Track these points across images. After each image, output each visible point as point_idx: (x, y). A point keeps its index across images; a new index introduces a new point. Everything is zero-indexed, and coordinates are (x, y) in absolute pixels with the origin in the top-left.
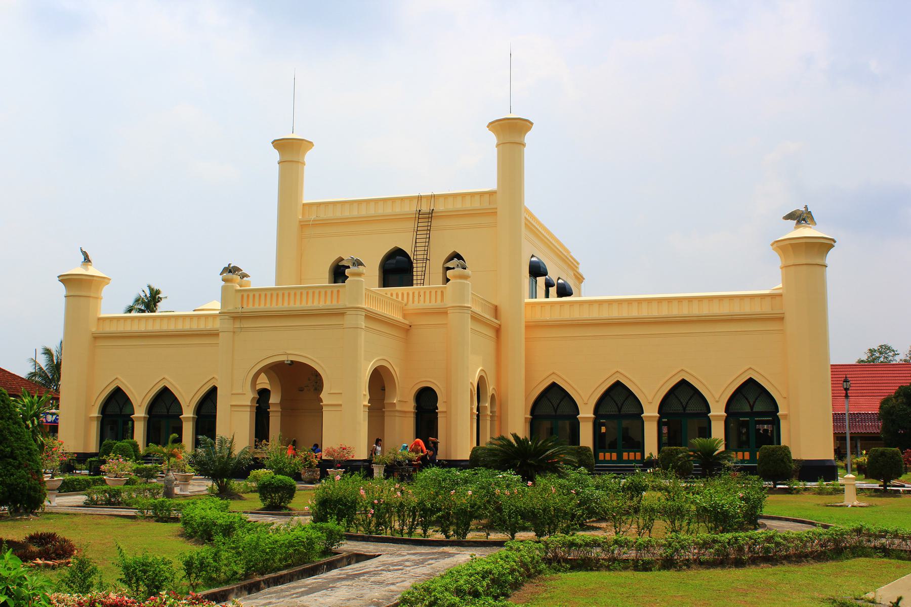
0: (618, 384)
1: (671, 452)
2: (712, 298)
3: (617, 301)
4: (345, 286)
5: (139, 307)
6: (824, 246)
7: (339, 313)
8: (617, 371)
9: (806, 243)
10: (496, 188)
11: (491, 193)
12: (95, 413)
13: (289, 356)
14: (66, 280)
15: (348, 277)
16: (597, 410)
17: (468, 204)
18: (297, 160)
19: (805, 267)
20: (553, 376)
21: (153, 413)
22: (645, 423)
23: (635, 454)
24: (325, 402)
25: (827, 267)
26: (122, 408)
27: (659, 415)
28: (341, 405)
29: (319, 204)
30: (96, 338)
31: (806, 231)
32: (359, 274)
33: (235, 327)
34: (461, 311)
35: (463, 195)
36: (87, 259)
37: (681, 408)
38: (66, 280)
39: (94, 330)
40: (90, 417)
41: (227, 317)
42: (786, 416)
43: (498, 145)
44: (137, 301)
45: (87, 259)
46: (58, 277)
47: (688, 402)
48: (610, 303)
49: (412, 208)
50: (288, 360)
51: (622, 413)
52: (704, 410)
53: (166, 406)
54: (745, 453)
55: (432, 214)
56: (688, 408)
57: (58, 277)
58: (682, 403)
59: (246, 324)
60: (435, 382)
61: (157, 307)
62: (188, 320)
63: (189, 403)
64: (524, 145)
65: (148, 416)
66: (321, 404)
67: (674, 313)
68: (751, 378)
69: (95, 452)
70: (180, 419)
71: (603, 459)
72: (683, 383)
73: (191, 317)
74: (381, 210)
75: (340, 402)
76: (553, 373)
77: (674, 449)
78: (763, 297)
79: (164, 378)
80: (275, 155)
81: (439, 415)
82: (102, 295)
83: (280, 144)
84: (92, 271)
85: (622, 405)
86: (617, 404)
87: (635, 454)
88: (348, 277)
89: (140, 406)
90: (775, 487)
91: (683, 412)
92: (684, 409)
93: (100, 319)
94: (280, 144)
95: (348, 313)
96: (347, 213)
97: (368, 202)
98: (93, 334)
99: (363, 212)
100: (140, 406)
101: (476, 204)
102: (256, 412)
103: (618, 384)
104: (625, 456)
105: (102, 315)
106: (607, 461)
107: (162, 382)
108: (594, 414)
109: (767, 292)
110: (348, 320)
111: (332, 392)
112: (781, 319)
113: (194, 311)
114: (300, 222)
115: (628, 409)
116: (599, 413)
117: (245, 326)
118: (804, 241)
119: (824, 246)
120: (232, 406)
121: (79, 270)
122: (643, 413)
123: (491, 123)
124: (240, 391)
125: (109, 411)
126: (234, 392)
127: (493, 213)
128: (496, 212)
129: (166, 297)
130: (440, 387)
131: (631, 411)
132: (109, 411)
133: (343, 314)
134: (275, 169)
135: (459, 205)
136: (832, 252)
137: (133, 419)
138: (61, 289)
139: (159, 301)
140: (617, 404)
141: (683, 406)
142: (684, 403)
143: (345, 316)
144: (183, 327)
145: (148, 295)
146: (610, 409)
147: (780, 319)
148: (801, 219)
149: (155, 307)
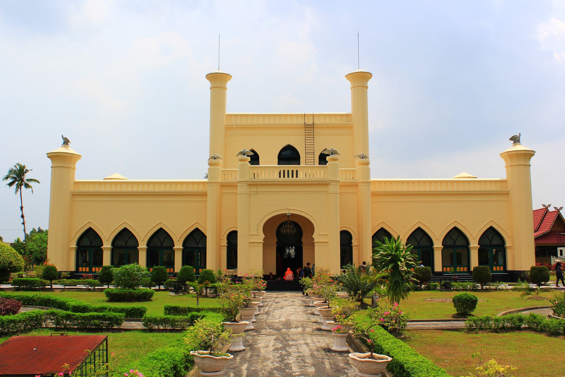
0: (161, 230)
1: (541, 269)
2: (166, 183)
3: (451, 181)
4: (327, 167)
5: (12, 176)
6: (529, 155)
7: (325, 184)
8: (383, 222)
9: (525, 153)
10: (351, 112)
11: (347, 115)
12: (74, 246)
13: (290, 210)
14: (53, 156)
15: (328, 162)
16: (113, 243)
17: (333, 121)
18: (224, 87)
19: (523, 166)
20: (125, 224)
21: (80, 245)
22: (139, 252)
23: (464, 268)
24: (316, 240)
25: (530, 166)
26: (92, 242)
27: (182, 247)
28: (328, 242)
29: (237, 115)
30: (74, 195)
31: (518, 147)
32: (336, 160)
33: (250, 190)
34: (210, 185)
35: (286, 116)
36: (66, 142)
37: (453, 243)
38: (53, 156)
39: (72, 190)
40: (71, 248)
41: (245, 184)
42: (510, 247)
43: (211, 88)
44: (11, 172)
45: (66, 142)
46: (47, 154)
47: (456, 239)
48: (374, 182)
49: (301, 121)
50: (289, 214)
51: (163, 246)
52: (464, 243)
53: (125, 241)
54: (497, 267)
55: (313, 125)
56: (456, 243)
57: (47, 154)
58: (453, 240)
59: (260, 189)
60: (350, 227)
61: (24, 176)
62: (174, 186)
63: (180, 239)
64: (367, 87)
65: (112, 247)
66: (314, 241)
67: (140, 190)
68: (197, 228)
69: (74, 270)
70: (137, 249)
71: (81, 271)
72: (197, 230)
73: (100, 183)
74: (283, 121)
75: (327, 240)
76: (455, 221)
77: (542, 267)
78: (496, 182)
79: (197, 223)
80: (208, 84)
81: (353, 248)
82: (76, 166)
83: (212, 77)
84: (70, 150)
85: (163, 241)
86: (417, 241)
87: (464, 268)
88: (328, 162)
89: (179, 241)
90: (482, 287)
91: (161, 246)
92: (454, 243)
93: (76, 183)
94: (212, 77)
95: (332, 184)
96: (255, 122)
97: (269, 116)
98: (72, 192)
99: (266, 121)
100: (179, 241)
101: (338, 121)
102: (228, 247)
103: (161, 230)
104: (94, 269)
105: (77, 180)
106: (171, 273)
107: (124, 224)
108: (183, 246)
109: (498, 179)
110: (332, 188)
111: (321, 233)
112: (507, 194)
113: (104, 179)
114: (225, 126)
115: (131, 243)
116: (115, 245)
117: (259, 191)
118: (524, 152)
119: (529, 155)
120: (250, 242)
121: (63, 150)
122: (174, 246)
123: (207, 75)
124: (256, 233)
125: (82, 244)
126: (251, 233)
127: (351, 127)
128: (352, 127)
129: (32, 170)
130: (354, 230)
131: (425, 244)
132: (118, 243)
133: (328, 185)
134: (208, 92)
135: (328, 121)
136: (533, 158)
137: (103, 249)
138: (49, 162)
139: (26, 172)
140: (417, 241)
141: (454, 241)
142: (454, 240)
143: (329, 186)
144: (115, 190)
145: (19, 169)
146: (121, 243)
147: (507, 194)
148: (516, 140)
149: (23, 176)
